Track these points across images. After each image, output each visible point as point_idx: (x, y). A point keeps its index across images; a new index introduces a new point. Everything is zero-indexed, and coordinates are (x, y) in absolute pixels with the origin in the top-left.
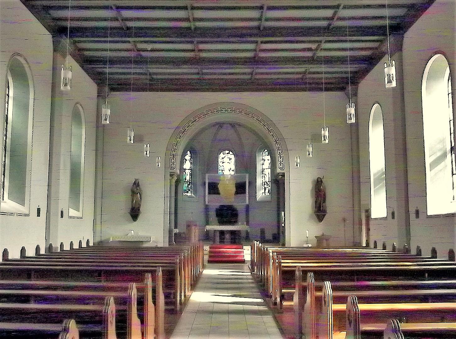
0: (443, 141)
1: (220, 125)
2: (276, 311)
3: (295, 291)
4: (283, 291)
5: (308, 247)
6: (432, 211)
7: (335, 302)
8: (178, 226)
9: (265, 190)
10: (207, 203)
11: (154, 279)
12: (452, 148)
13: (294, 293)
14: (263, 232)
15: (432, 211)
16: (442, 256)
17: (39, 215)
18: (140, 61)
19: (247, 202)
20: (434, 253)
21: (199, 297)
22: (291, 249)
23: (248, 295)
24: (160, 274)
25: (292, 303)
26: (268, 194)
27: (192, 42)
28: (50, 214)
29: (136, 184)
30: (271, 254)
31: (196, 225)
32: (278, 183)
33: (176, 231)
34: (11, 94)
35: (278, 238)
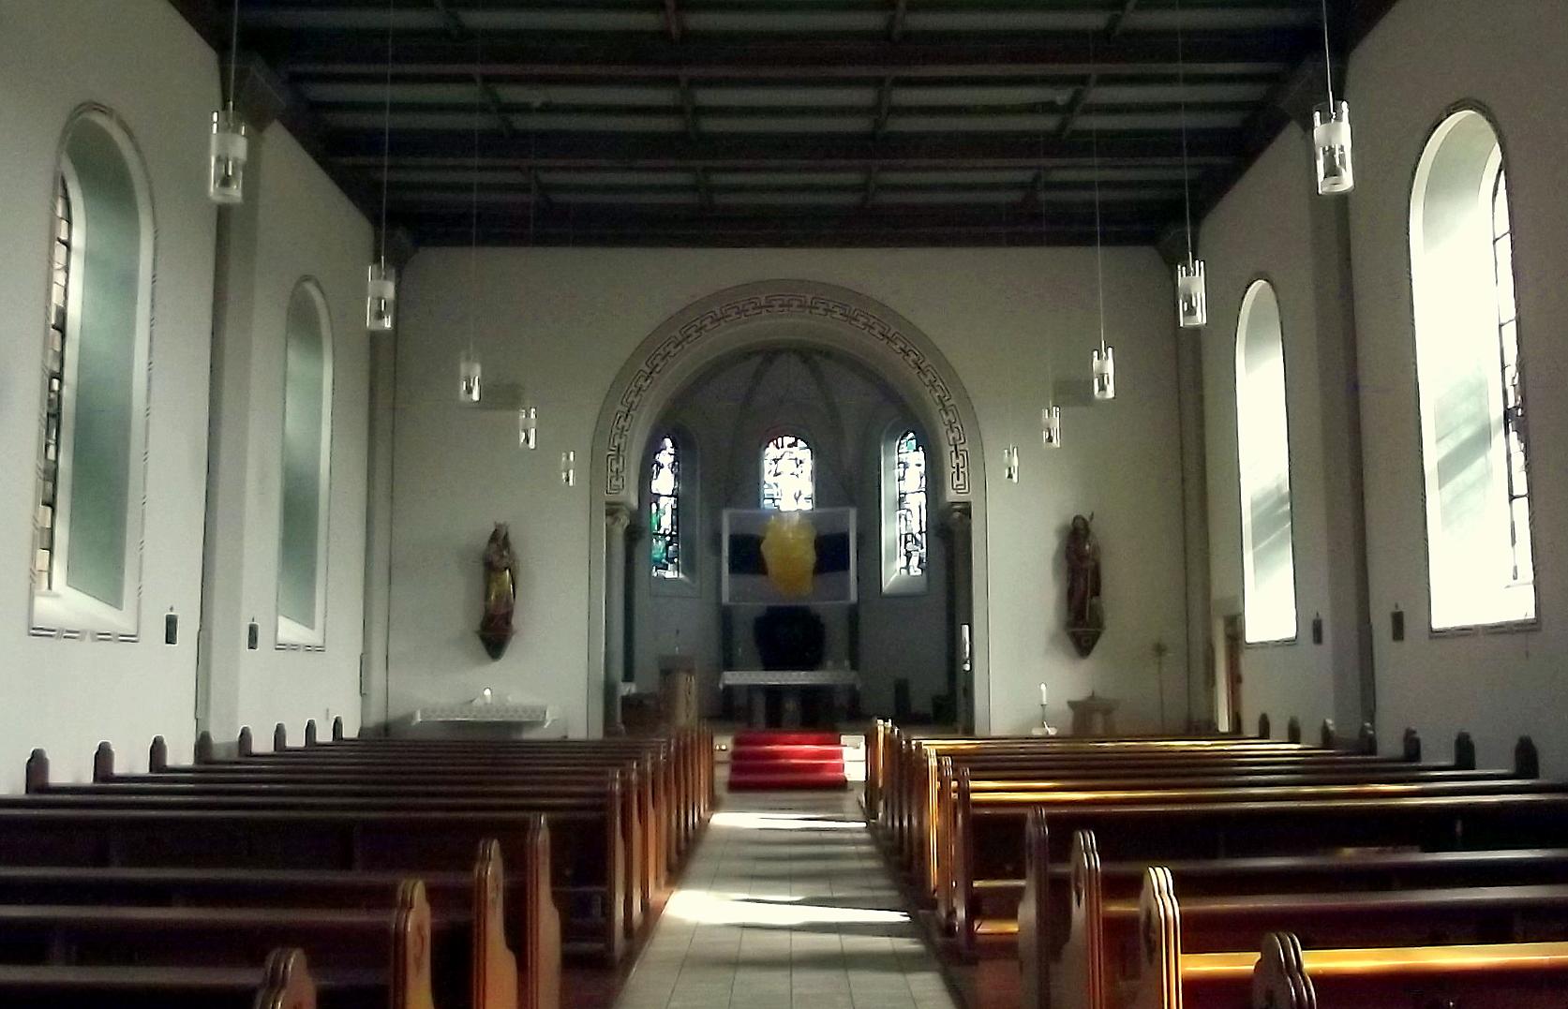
0: (1478, 390)
1: (770, 353)
2: (952, 953)
3: (1021, 883)
4: (976, 884)
5: (1047, 737)
6: (1445, 614)
7: (1191, 946)
8: (637, 672)
9: (909, 559)
10: (725, 599)
11: (517, 862)
12: (1507, 414)
13: (1020, 890)
14: (902, 689)
15: (1445, 614)
16: (1495, 762)
17: (170, 638)
18: (505, 143)
19: (853, 597)
20: (1465, 754)
21: (694, 908)
22: (991, 745)
23: (860, 899)
24: (543, 838)
25: (1012, 927)
26: (919, 572)
27: (672, 82)
28: (208, 635)
29: (500, 540)
30: (933, 763)
31: (690, 672)
32: (950, 535)
33: (627, 689)
34: (78, 240)
35: (950, 708)
